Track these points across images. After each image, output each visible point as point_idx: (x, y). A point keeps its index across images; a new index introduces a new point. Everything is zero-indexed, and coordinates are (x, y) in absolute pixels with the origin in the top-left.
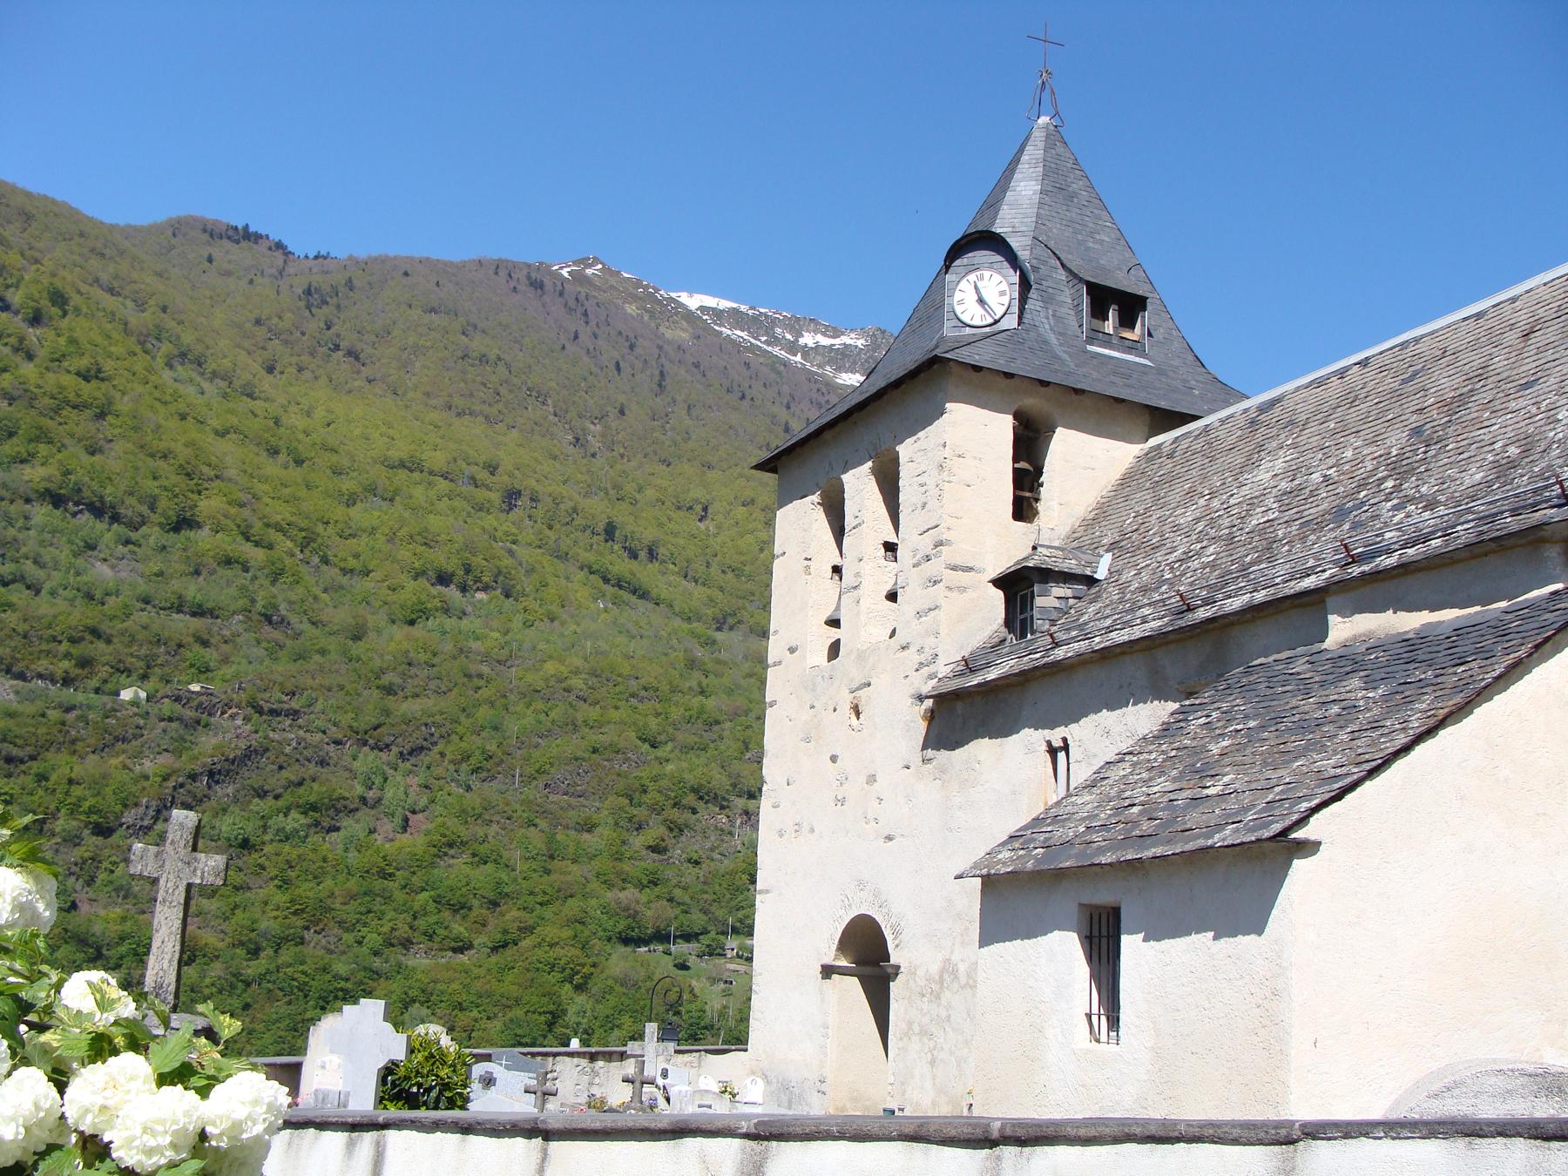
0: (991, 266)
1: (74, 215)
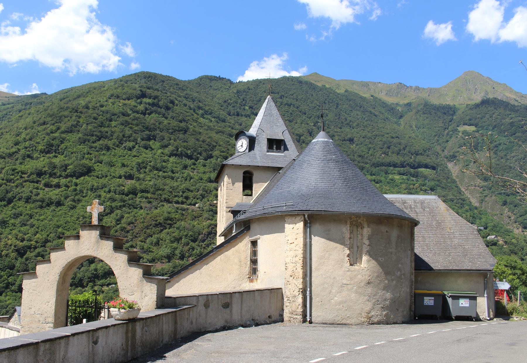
1: (174, 79)
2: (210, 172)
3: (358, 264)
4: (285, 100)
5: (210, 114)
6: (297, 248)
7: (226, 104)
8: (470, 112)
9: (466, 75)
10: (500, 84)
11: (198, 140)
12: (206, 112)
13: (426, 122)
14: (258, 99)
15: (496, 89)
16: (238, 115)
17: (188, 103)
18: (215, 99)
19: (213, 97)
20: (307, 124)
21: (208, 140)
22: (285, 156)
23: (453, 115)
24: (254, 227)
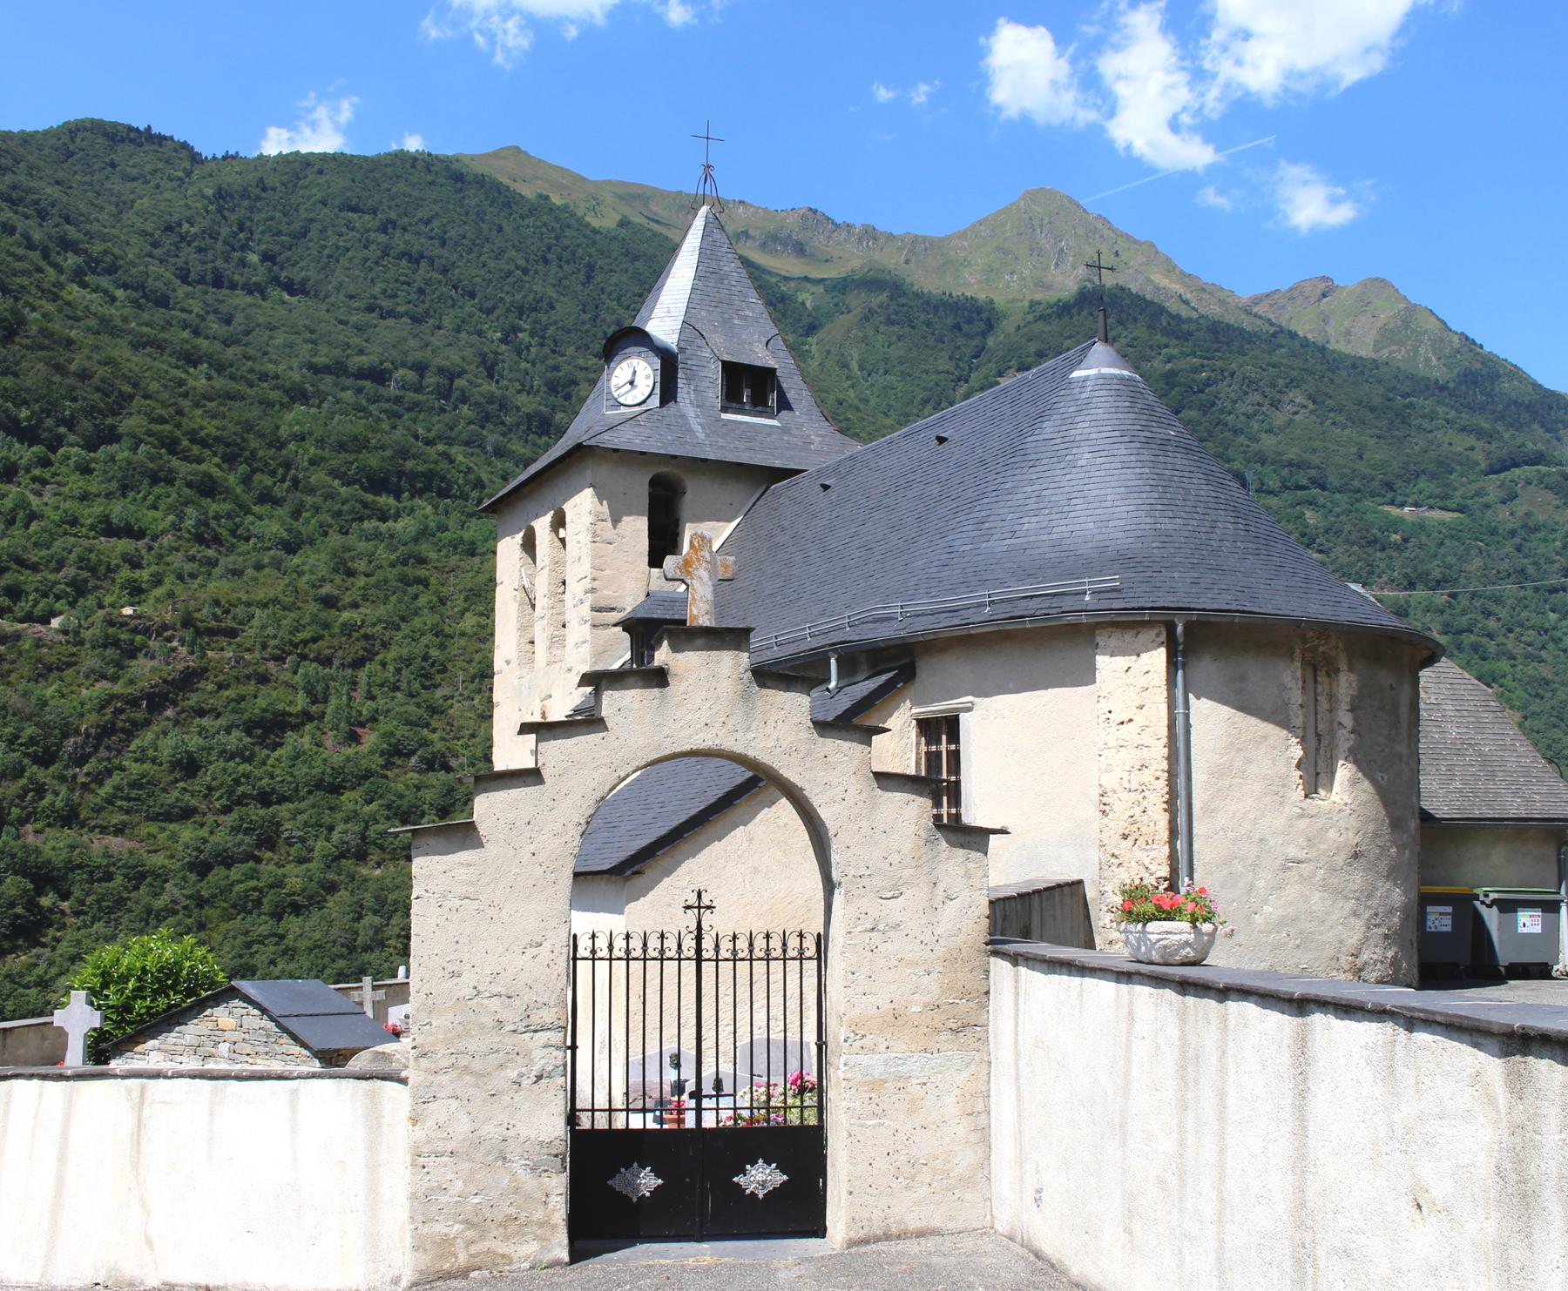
0: (639, 355)
2: (109, 495)
3: (1322, 792)
4: (399, 241)
5: (111, 270)
6: (1146, 738)
7: (174, 238)
8: (1039, 327)
9: (1033, 201)
10: (1135, 241)
11: (60, 369)
12: (92, 264)
13: (896, 352)
14: (296, 226)
15: (1124, 256)
16: (218, 282)
17: (21, 224)
18: (129, 217)
19: (122, 206)
20: (480, 333)
21: (103, 371)
22: (785, 430)
23: (984, 335)
24: (929, 671)
